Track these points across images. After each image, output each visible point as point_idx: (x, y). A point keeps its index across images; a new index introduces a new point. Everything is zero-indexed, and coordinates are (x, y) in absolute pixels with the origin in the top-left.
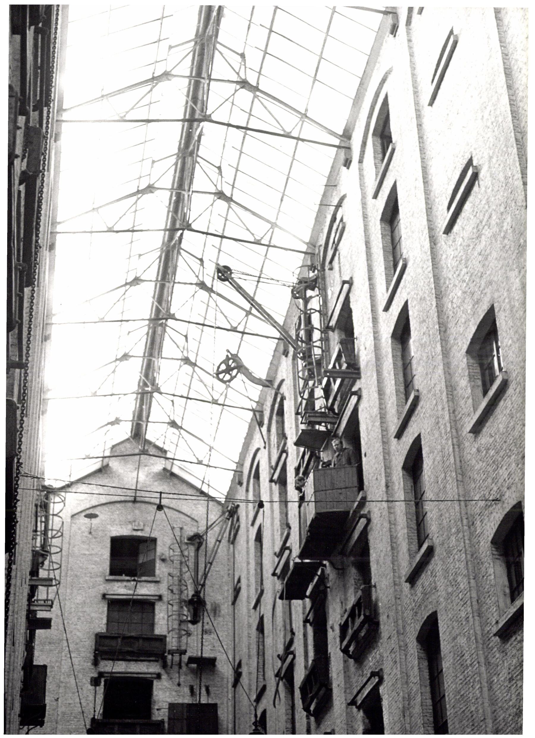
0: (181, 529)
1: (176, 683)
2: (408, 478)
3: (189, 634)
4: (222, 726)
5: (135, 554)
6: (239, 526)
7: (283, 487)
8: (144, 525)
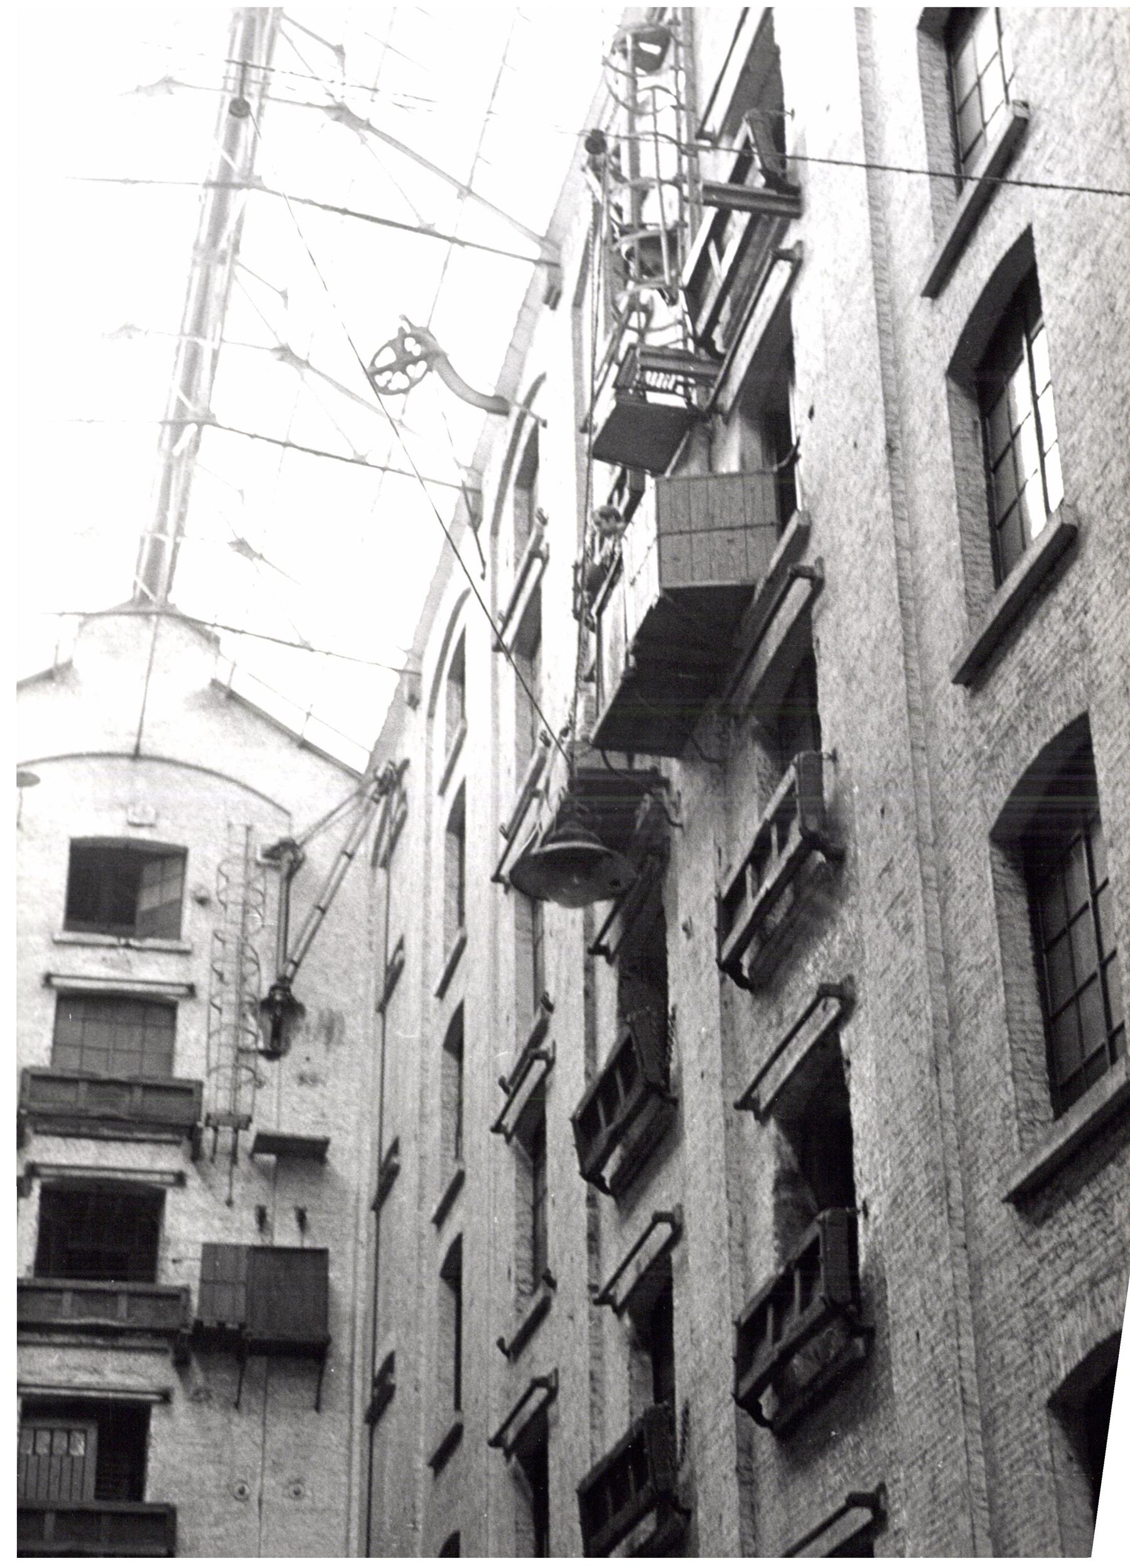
1: (223, 1198)
2: (964, 401)
3: (258, 1083)
4: (339, 1306)
6: (405, 815)
8: (157, 815)
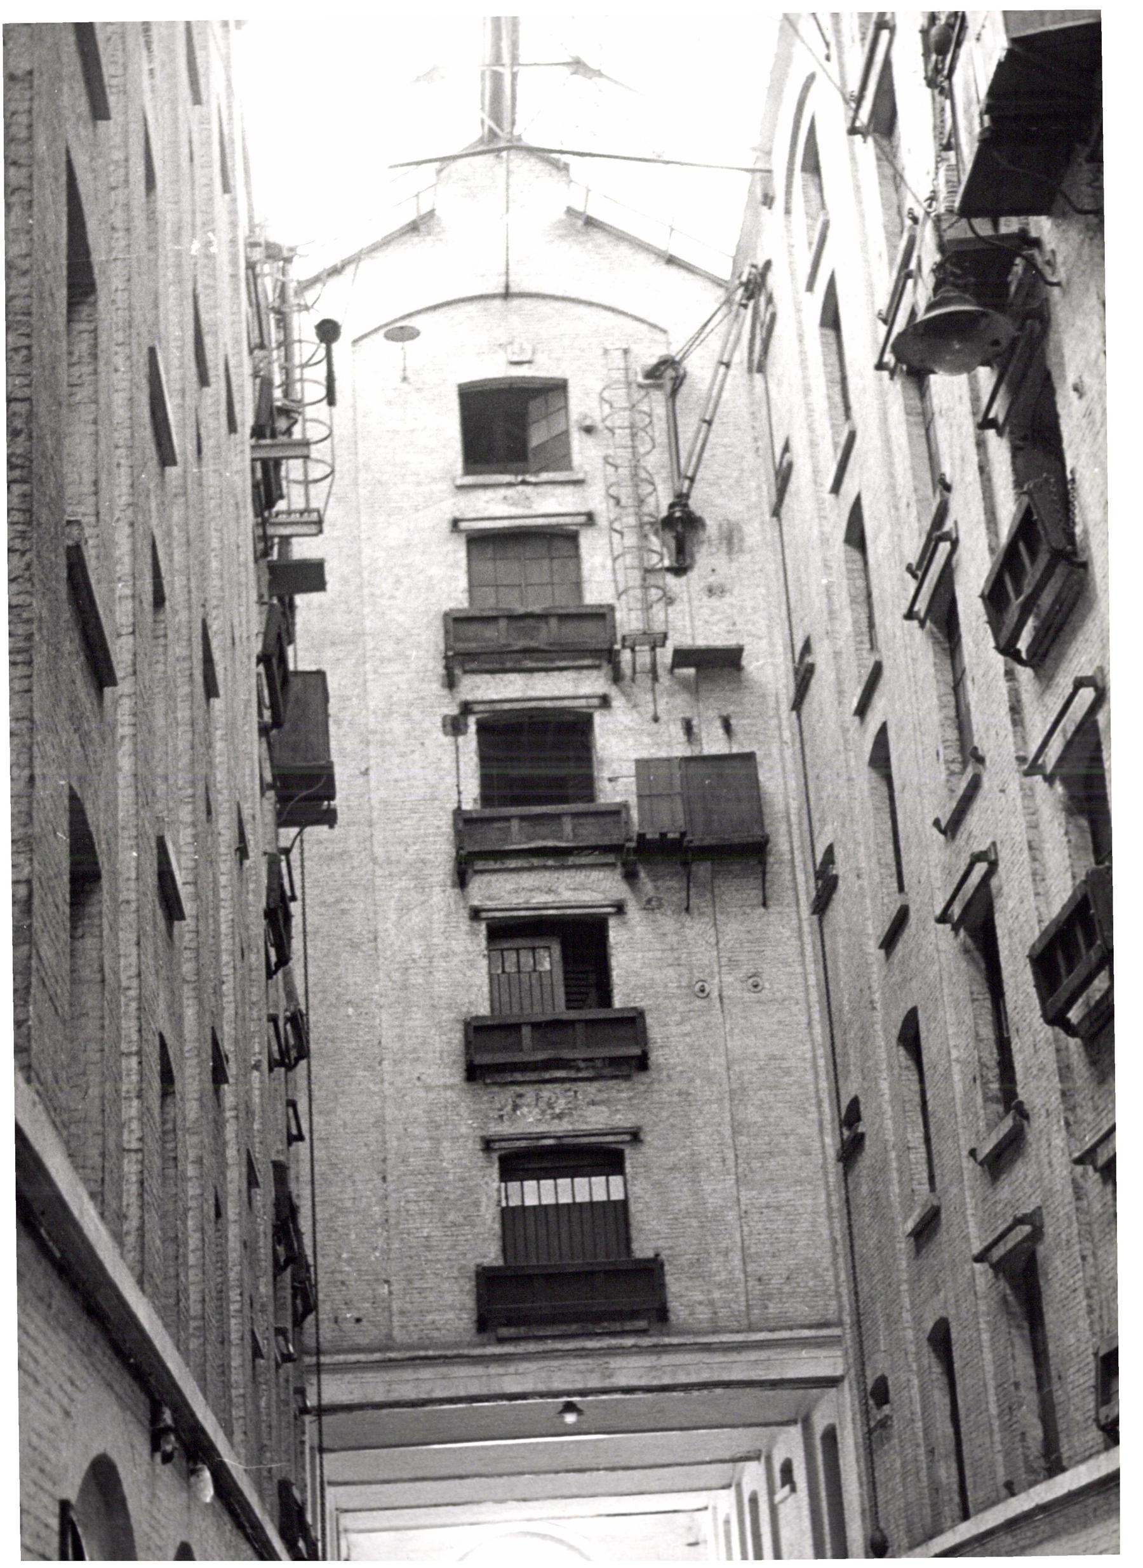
0: (626, 352)
1: (650, 715)
3: (669, 600)
4: (772, 806)
5: (520, 423)
6: (773, 317)
7: (884, 143)
8: (534, 353)
